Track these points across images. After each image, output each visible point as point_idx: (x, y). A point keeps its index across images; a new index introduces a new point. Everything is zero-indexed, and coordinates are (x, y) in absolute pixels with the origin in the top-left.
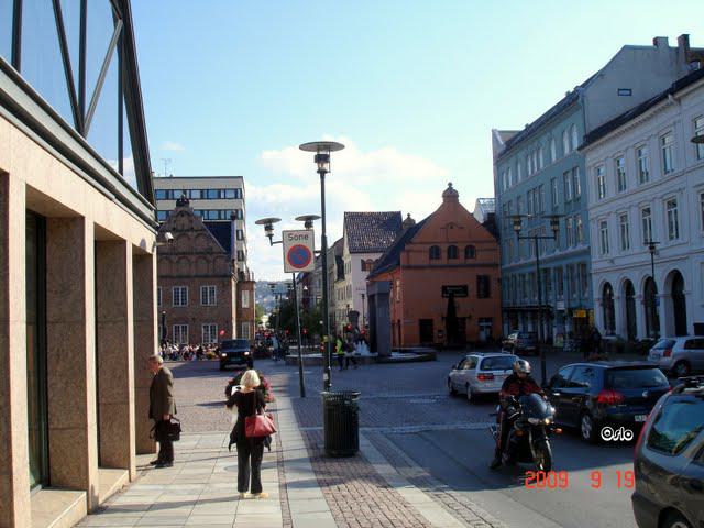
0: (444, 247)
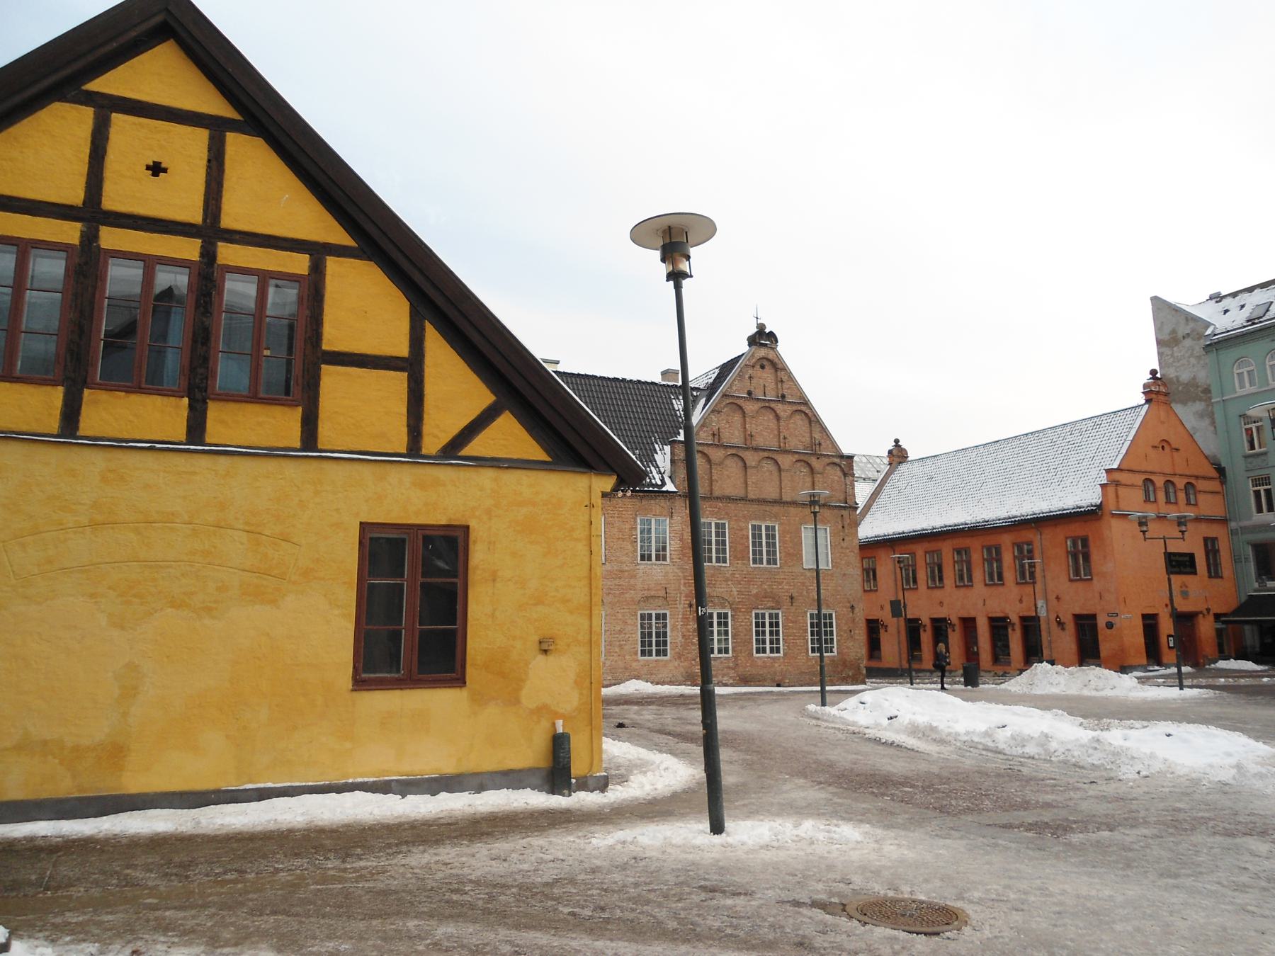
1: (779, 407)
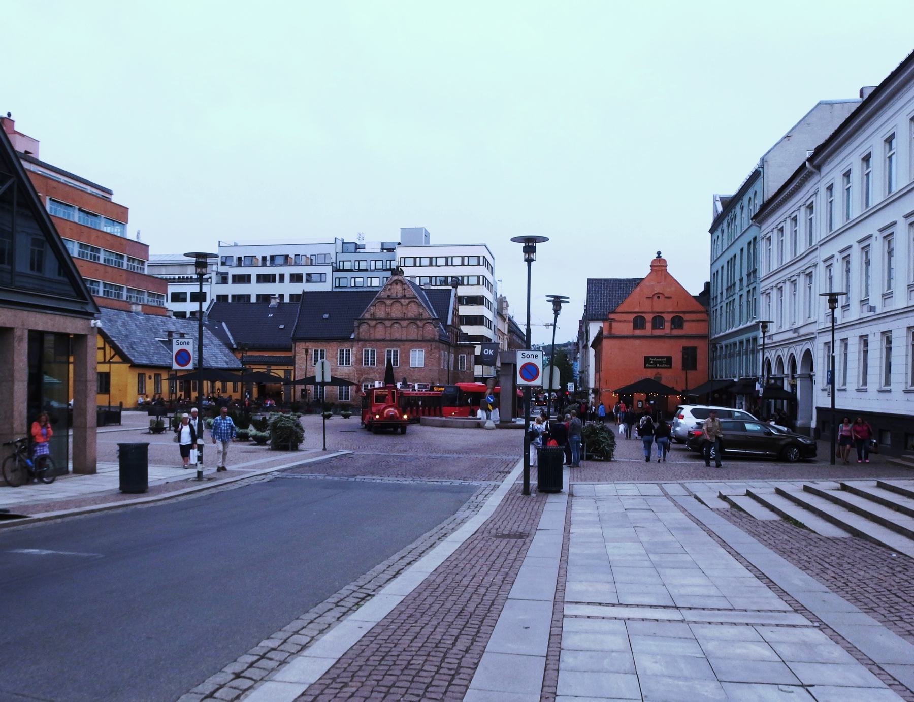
0: (649, 317)
1: (403, 301)
